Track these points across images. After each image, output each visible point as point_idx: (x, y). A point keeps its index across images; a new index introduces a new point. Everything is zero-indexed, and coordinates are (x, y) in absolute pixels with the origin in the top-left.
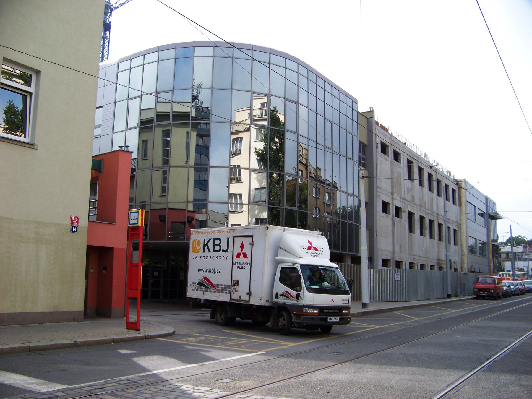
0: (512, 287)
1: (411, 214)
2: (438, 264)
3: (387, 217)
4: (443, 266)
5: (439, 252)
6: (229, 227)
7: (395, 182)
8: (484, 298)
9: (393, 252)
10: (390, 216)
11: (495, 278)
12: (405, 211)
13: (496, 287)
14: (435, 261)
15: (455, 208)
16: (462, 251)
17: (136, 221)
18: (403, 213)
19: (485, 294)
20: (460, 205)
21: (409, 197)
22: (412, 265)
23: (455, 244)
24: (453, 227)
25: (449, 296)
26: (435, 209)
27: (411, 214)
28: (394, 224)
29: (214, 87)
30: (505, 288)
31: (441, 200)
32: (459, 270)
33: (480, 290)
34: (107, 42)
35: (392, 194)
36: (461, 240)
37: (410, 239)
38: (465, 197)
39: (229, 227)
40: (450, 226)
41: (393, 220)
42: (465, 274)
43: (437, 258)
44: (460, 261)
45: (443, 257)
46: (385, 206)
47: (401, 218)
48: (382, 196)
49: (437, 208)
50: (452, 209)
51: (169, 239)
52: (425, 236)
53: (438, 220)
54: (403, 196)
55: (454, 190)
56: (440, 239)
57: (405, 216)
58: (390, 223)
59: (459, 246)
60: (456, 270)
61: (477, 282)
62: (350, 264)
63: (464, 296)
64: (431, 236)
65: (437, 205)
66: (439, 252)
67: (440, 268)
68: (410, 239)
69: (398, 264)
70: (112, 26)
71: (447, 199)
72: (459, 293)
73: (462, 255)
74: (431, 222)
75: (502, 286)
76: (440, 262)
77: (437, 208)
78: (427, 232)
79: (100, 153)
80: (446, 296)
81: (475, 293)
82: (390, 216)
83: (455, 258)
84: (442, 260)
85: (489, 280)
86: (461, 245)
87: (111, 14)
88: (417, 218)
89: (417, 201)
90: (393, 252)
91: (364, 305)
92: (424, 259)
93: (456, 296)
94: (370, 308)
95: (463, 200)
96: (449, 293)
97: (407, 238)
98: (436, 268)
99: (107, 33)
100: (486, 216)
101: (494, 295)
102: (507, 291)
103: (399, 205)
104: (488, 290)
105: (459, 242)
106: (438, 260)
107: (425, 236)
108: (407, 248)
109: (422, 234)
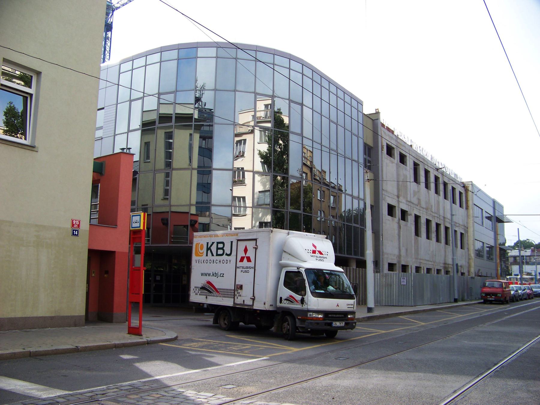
0: (520, 291)
1: (417, 218)
2: (445, 268)
3: (393, 220)
4: (450, 270)
5: (445, 256)
6: (232, 230)
7: (401, 185)
8: (491, 302)
9: (399, 256)
10: (396, 220)
11: (502, 283)
12: (411, 215)
13: (503, 291)
14: (442, 265)
15: (462, 211)
16: (469, 255)
17: (138, 225)
18: (409, 217)
19: (493, 298)
20: (467, 208)
21: (415, 200)
22: (418, 269)
23: (461, 248)
24: (459, 230)
25: (456, 301)
26: (441, 212)
27: (417, 218)
28: (400, 227)
29: (217, 88)
30: (512, 292)
31: (448, 203)
32: (466, 274)
33: (487, 294)
34: (108, 43)
35: (398, 197)
36: (468, 244)
37: (416, 242)
38: (472, 200)
39: (232, 230)
40: (457, 229)
41: (399, 223)
42: (472, 278)
43: (443, 262)
44: (467, 265)
45: (450, 261)
46: (391, 209)
47: (408, 221)
48: (388, 199)
49: (444, 211)
50: (459, 212)
51: (171, 242)
52: (431, 240)
53: (444, 224)
54: (409, 199)
55: (460, 193)
56: (447, 243)
57: (411, 219)
58: (396, 226)
59: (466, 250)
60: (463, 274)
61: (484, 286)
62: (355, 268)
63: (471, 300)
64: (438, 240)
65: (444, 208)
66: (445, 256)
67: (447, 272)
68: (416, 242)
69: (404, 268)
70: (113, 26)
71: (454, 202)
72: (466, 298)
73: (469, 259)
74: (438, 225)
75: (510, 290)
76: (447, 266)
77: (444, 211)
78: (433, 235)
79: (102, 156)
80: (453, 300)
81: (482, 298)
82: (396, 220)
83: (461, 262)
84: (448, 264)
85: (496, 285)
86: (468, 249)
87: (113, 14)
88: (423, 221)
89: (423, 204)
90: (399, 256)
91: (370, 310)
92: (430, 263)
93: (463, 300)
94: (376, 313)
95: (470, 203)
96: (456, 297)
97: (413, 242)
98: (443, 272)
99: (109, 34)
100: (493, 219)
101: (502, 299)
102: (514, 295)
103: (405, 208)
104: (495, 294)
105: (466, 246)
106: (445, 264)
107: (431, 240)
108: (413, 252)
109: (428, 237)
